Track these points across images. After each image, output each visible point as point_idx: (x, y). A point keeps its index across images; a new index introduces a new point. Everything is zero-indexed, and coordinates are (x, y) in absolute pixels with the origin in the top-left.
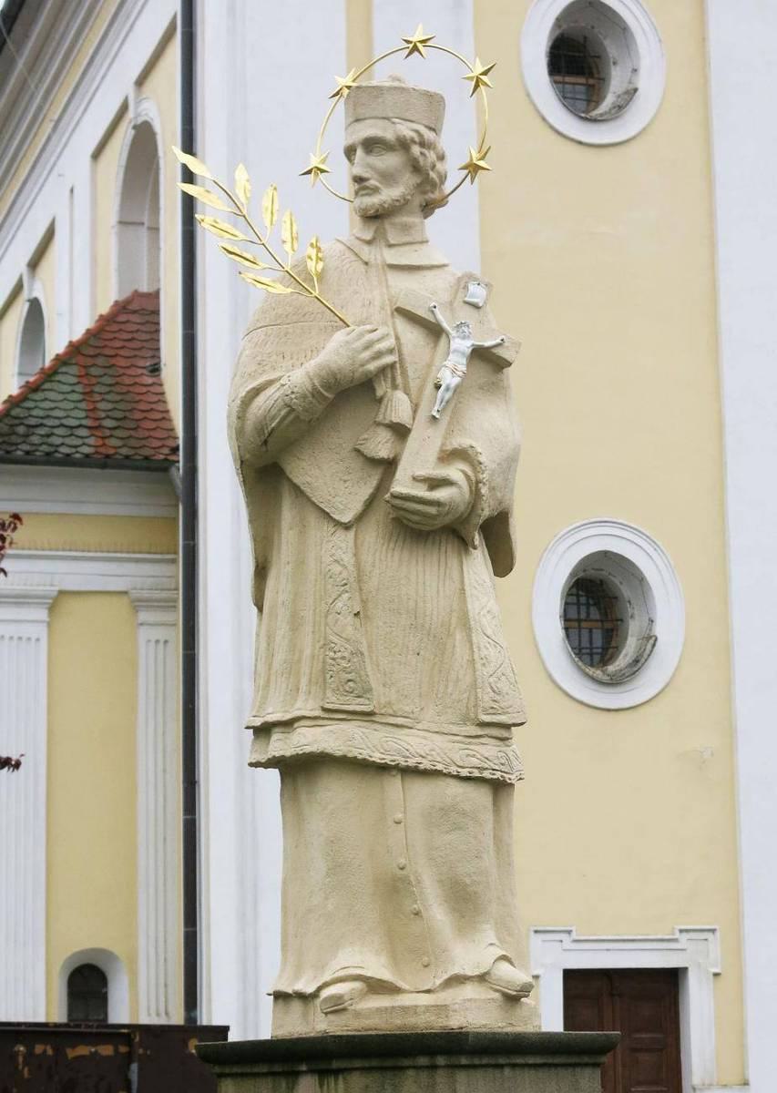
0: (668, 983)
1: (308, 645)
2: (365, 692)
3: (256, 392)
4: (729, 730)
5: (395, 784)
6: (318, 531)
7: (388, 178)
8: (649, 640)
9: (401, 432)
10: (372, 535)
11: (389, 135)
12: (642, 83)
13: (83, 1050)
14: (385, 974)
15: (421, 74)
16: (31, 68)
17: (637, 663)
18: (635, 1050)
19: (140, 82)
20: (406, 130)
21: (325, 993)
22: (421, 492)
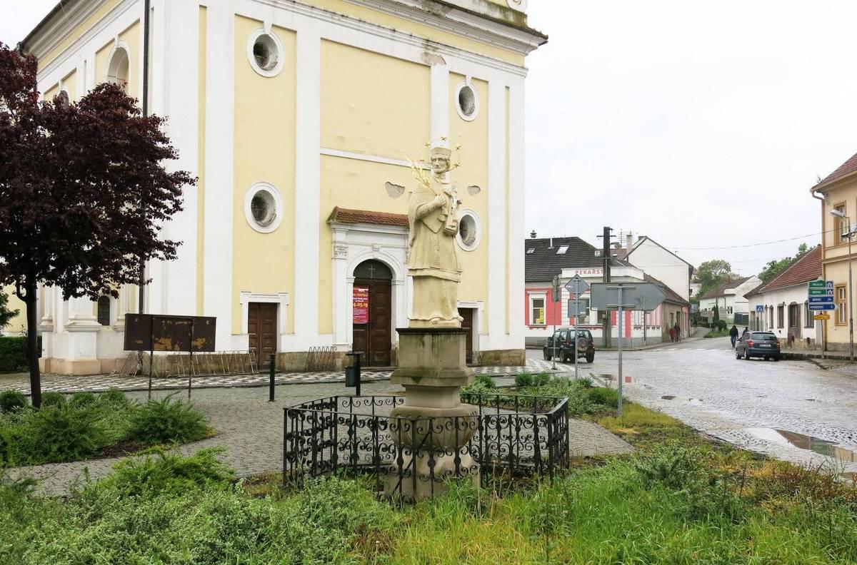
0: (274, 306)
1: (427, 255)
2: (439, 265)
3: (420, 206)
4: (294, 242)
5: (443, 281)
6: (429, 233)
7: (442, 166)
8: (274, 215)
9: (446, 216)
10: (440, 235)
11: (444, 158)
12: (279, 60)
13: (180, 323)
14: (442, 316)
15: (446, 145)
16: (70, 17)
17: (270, 221)
18: (265, 324)
19: (120, 35)
20: (447, 157)
21: (433, 320)
22: (450, 228)
